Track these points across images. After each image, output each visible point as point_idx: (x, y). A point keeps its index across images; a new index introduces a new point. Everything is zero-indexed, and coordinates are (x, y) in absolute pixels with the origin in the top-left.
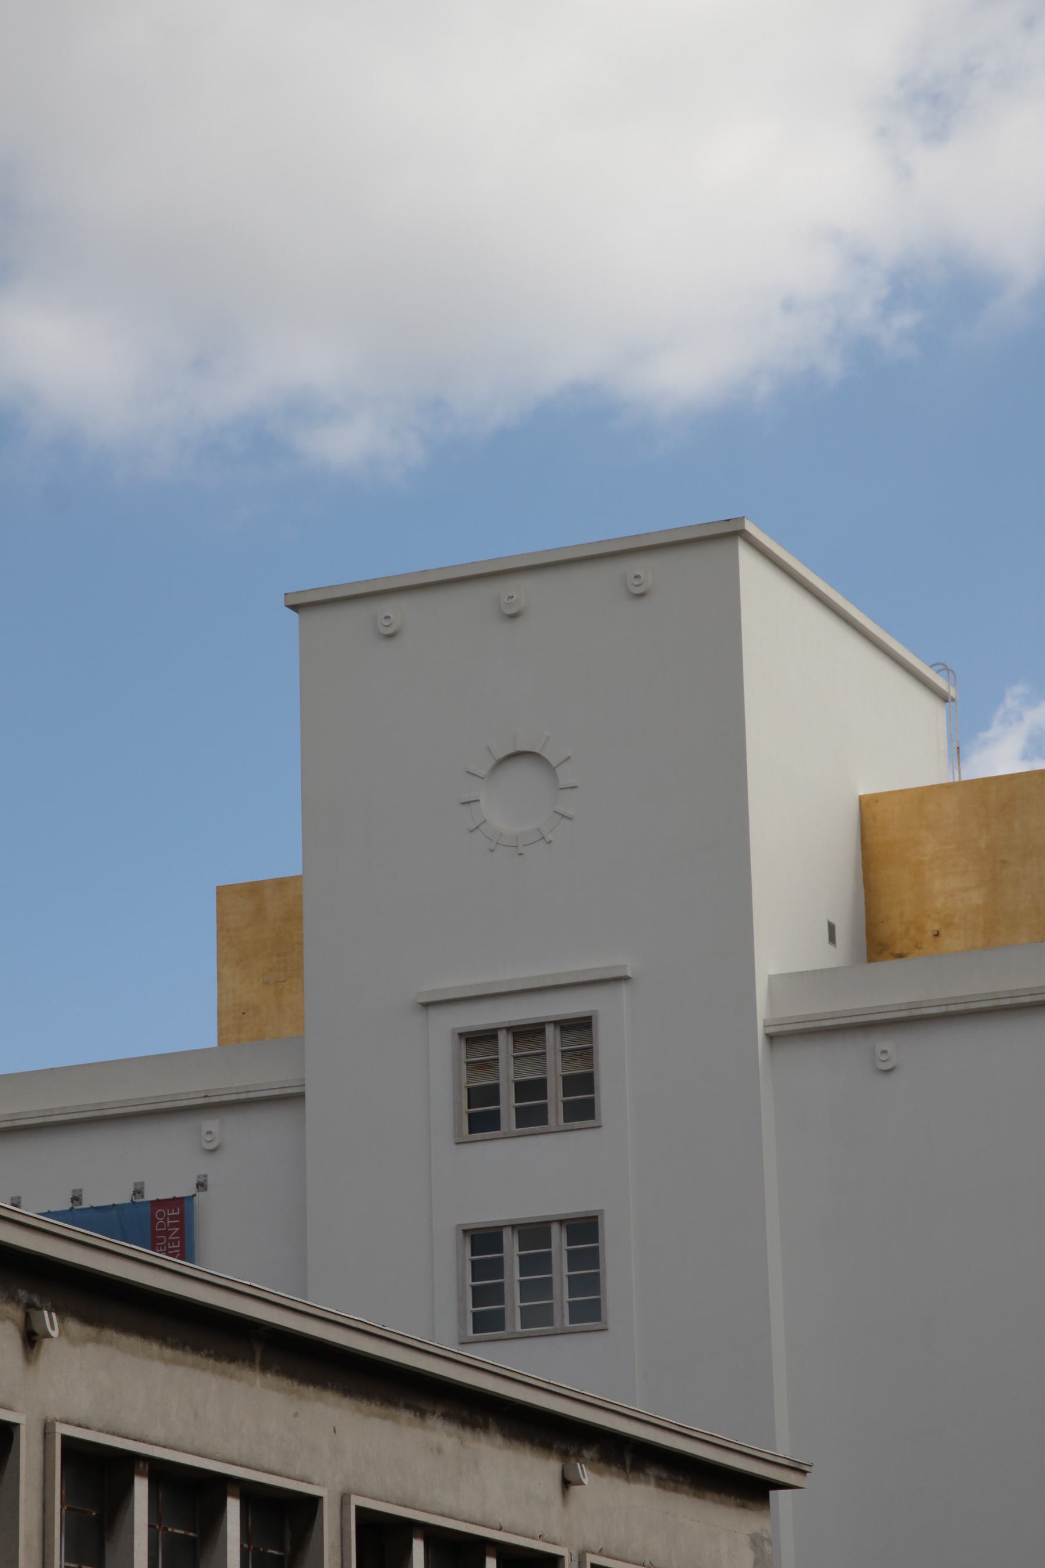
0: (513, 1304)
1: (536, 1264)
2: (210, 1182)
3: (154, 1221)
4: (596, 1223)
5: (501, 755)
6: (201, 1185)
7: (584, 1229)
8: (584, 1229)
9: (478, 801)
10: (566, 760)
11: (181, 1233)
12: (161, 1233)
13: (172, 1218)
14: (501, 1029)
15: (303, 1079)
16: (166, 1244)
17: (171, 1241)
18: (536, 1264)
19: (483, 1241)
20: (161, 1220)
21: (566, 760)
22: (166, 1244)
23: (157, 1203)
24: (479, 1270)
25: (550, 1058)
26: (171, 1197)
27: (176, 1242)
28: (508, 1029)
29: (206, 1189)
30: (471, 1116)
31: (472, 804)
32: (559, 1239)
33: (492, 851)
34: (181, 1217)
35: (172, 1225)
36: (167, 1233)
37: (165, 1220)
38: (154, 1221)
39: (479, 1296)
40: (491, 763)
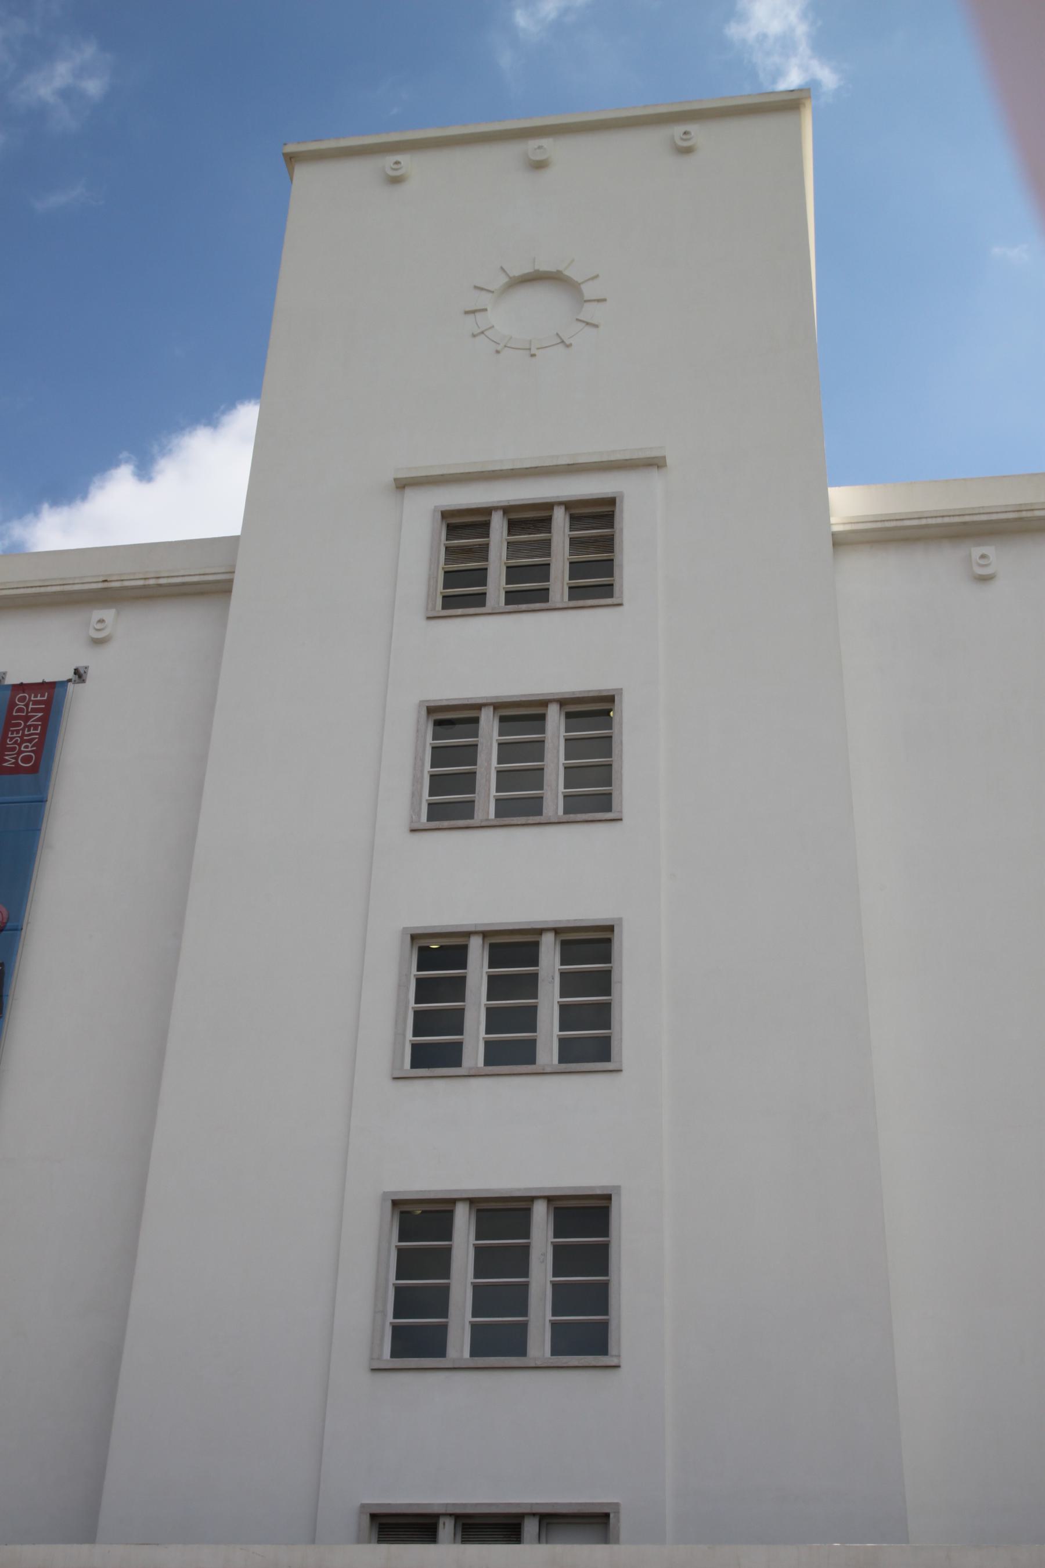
0: (489, 764)
1: (502, 1260)
2: (90, 677)
3: (12, 705)
4: (609, 941)
5: (516, 272)
6: (80, 675)
7: (586, 1218)
8: (586, 1218)
9: (486, 310)
10: (598, 301)
11: (45, 720)
12: (17, 718)
13: (35, 703)
14: (496, 508)
15: (234, 566)
16: (23, 729)
17: (29, 727)
18: (502, 1260)
19: (421, 1221)
20: (21, 705)
21: (598, 301)
22: (23, 729)
23: (22, 687)
24: (408, 1264)
25: (543, 988)
26: (40, 681)
27: (36, 727)
28: (472, 1201)
29: (84, 681)
30: (420, 982)
31: (478, 315)
32: (555, 728)
33: (498, 352)
34: (48, 703)
35: (34, 710)
36: (27, 718)
37: (27, 705)
38: (12, 705)
39: (405, 1302)
40: (503, 280)
